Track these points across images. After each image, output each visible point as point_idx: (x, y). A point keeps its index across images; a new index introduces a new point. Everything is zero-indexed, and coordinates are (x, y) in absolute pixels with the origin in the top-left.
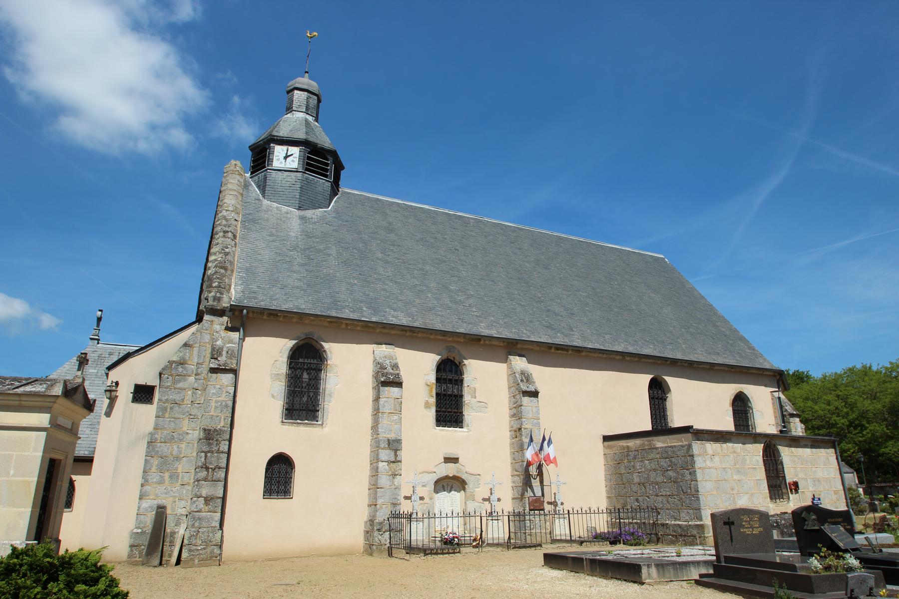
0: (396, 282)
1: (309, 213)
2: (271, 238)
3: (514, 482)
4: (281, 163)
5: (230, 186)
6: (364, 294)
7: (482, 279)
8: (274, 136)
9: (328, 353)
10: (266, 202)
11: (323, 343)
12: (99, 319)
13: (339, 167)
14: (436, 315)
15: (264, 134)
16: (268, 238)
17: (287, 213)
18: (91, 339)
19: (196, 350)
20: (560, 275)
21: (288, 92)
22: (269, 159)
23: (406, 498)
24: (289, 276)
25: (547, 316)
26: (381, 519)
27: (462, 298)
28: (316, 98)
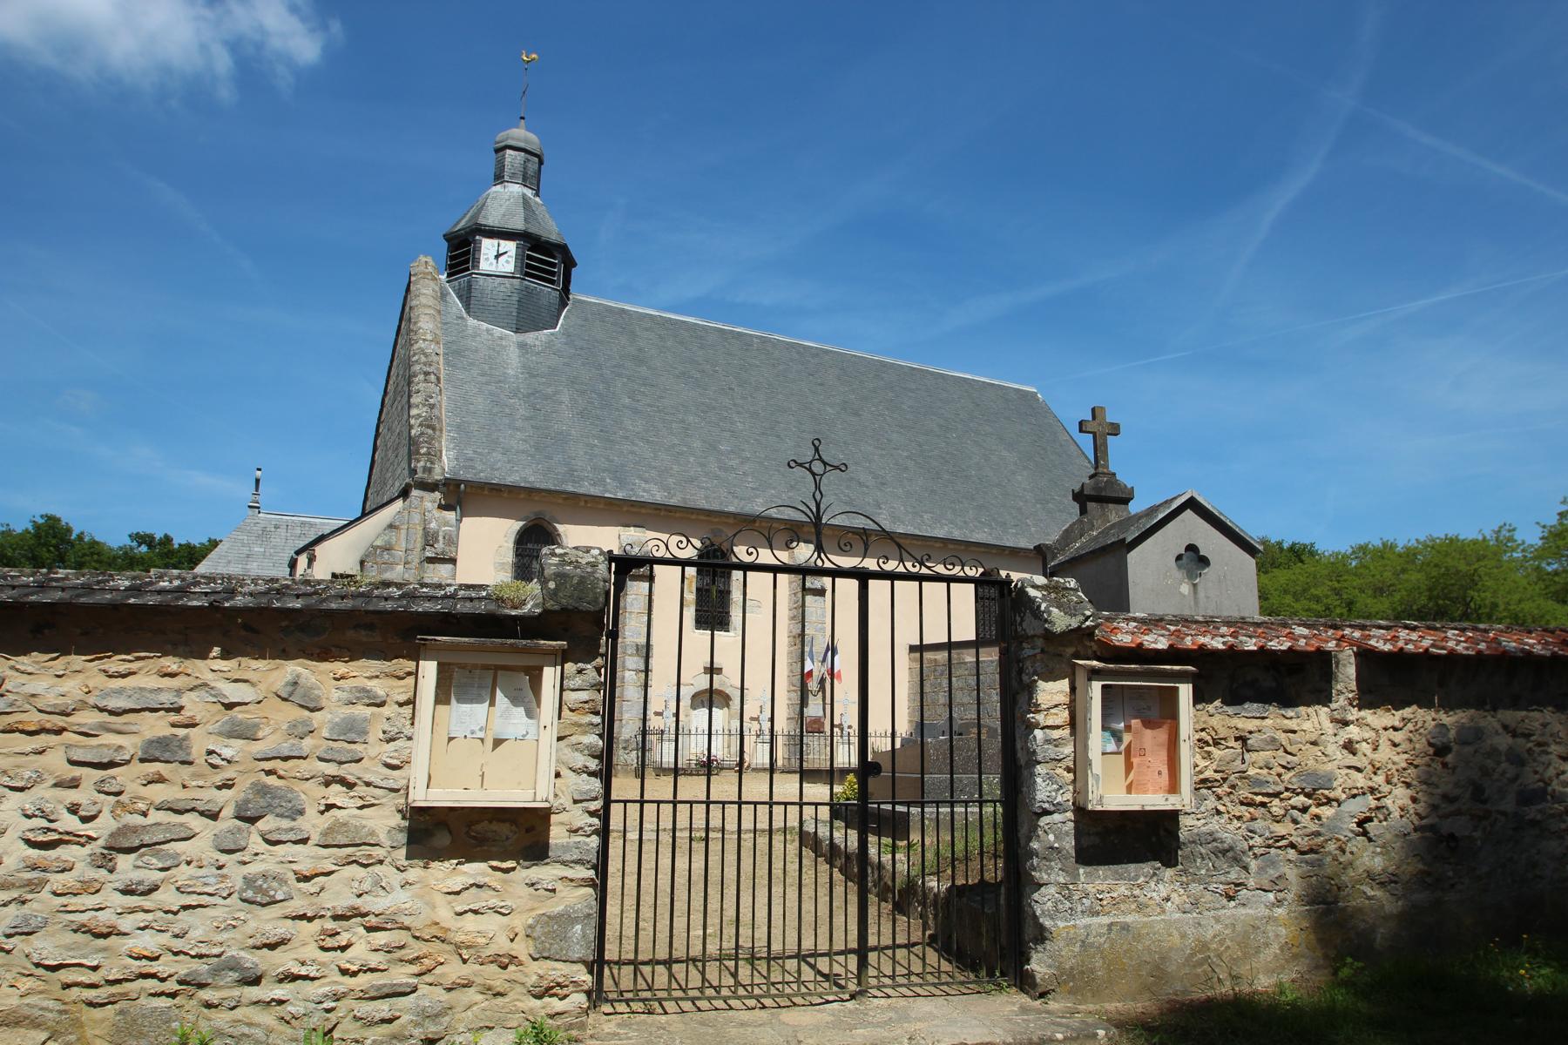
0: (648, 441)
1: (530, 337)
2: (484, 379)
3: (790, 699)
4: (491, 264)
5: (423, 300)
6: (608, 460)
7: (763, 434)
8: (481, 225)
9: (563, 537)
10: (471, 322)
11: (557, 525)
12: (258, 481)
13: (569, 263)
14: (699, 487)
15: (464, 217)
16: (480, 379)
17: (501, 338)
18: (250, 507)
19: (403, 532)
20: (874, 424)
21: (497, 151)
22: (474, 258)
23: (657, 714)
24: (511, 436)
25: (848, 487)
26: (628, 737)
27: (734, 463)
28: (536, 160)
